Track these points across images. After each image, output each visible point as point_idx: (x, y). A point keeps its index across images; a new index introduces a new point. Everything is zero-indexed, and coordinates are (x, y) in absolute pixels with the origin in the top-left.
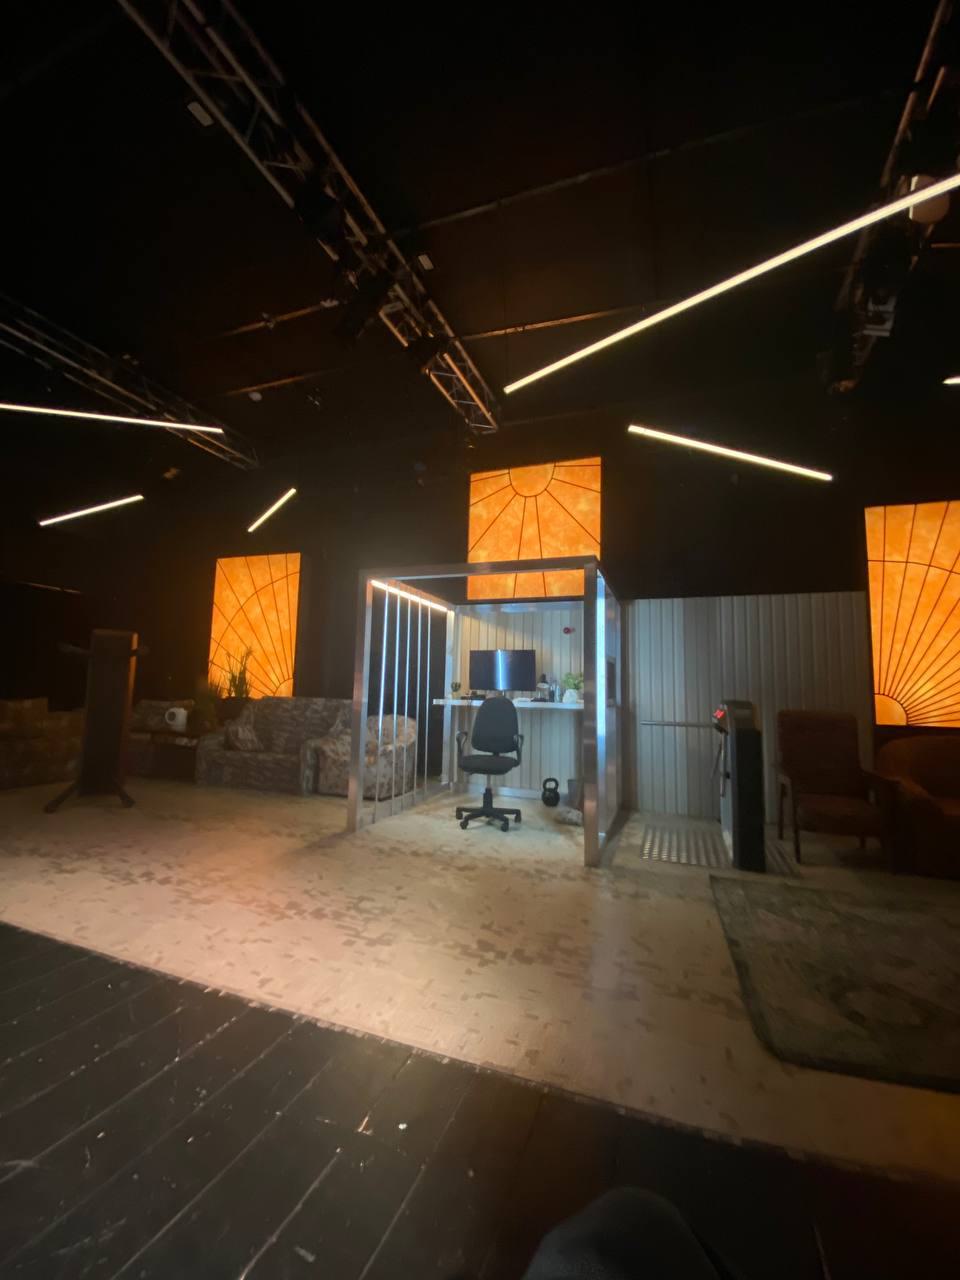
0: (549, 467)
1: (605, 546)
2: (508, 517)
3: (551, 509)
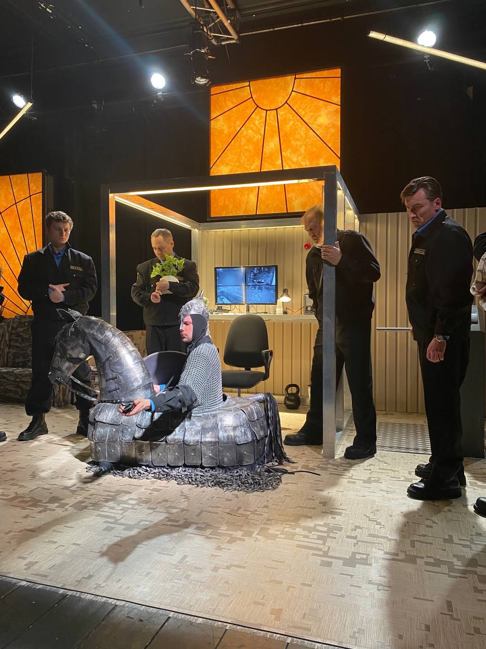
0: (290, 79)
1: (344, 158)
2: (250, 131)
3: (292, 123)
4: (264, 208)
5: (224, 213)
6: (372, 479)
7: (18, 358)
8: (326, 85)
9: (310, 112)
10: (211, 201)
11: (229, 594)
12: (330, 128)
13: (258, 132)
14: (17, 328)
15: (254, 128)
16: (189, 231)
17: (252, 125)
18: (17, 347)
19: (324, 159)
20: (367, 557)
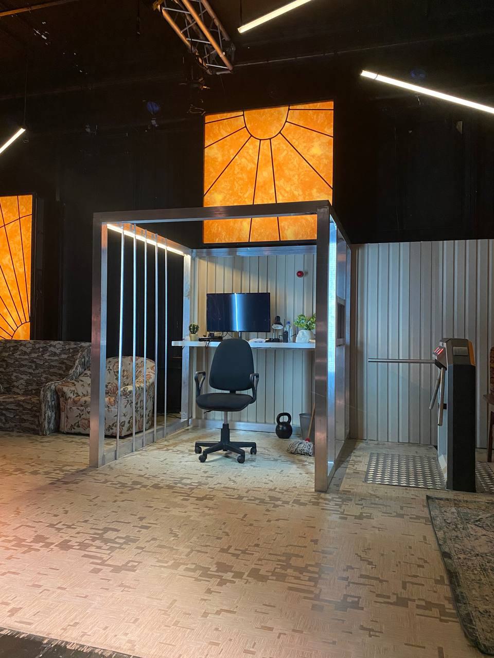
0: (283, 109)
3: (285, 152)
4: (257, 236)
5: (217, 239)
6: (364, 514)
7: (31, 385)
8: (319, 117)
9: (304, 142)
10: (205, 227)
11: (220, 642)
12: (322, 158)
13: (252, 161)
14: (60, 354)
15: (248, 157)
16: (182, 257)
17: (246, 154)
18: (31, 373)
19: (317, 189)
20: (359, 600)
